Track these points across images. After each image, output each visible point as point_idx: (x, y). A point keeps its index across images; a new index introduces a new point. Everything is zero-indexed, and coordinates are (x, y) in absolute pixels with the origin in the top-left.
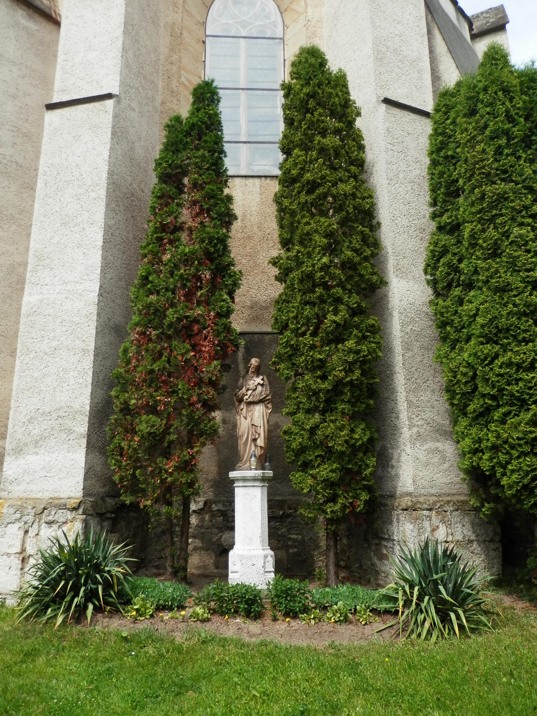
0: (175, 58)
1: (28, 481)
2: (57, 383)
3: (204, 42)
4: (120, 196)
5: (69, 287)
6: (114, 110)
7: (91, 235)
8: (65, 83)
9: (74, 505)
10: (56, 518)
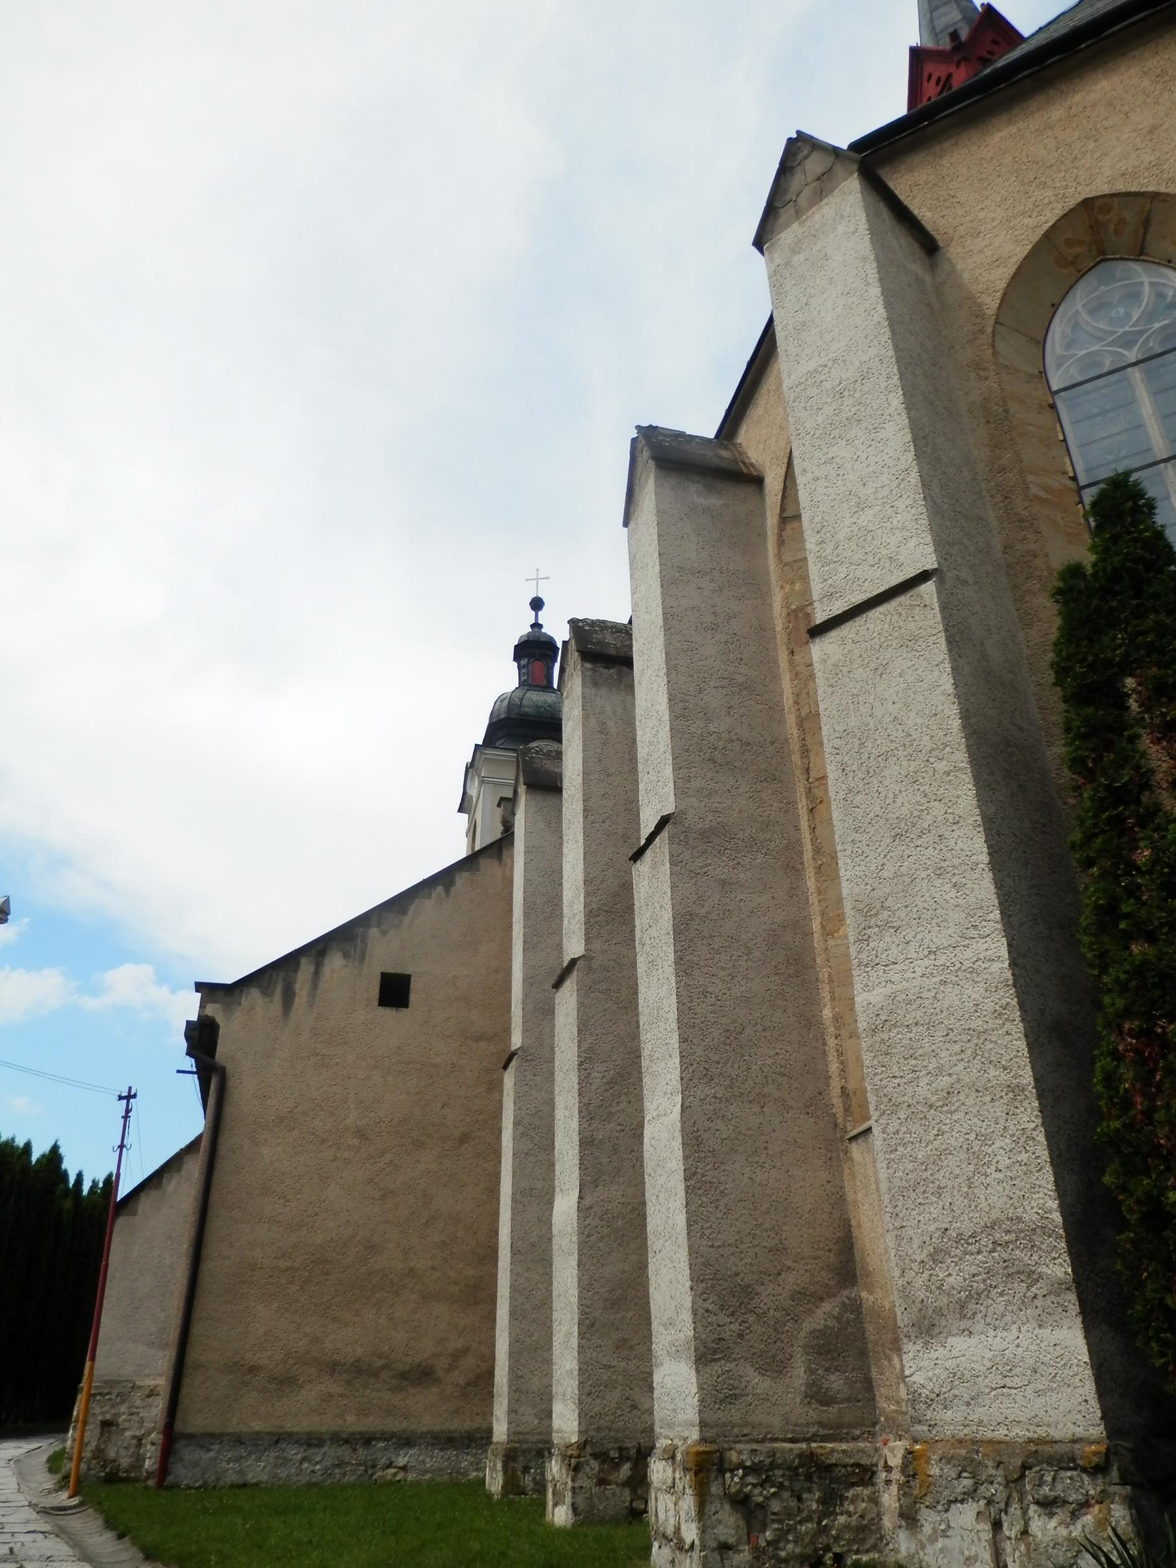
0: (1007, 457)
1: (966, 1397)
2: (972, 1168)
3: (1053, 407)
4: (998, 757)
5: (942, 960)
6: (939, 598)
7: (960, 844)
8: (830, 581)
9: (1096, 1460)
10: (1059, 1491)
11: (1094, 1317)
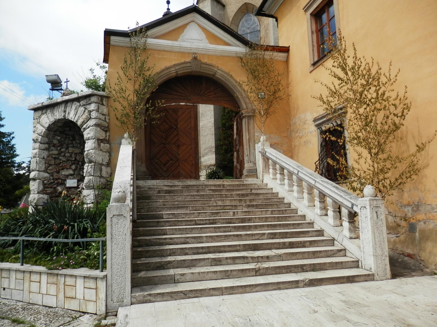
11: (216, 154)
